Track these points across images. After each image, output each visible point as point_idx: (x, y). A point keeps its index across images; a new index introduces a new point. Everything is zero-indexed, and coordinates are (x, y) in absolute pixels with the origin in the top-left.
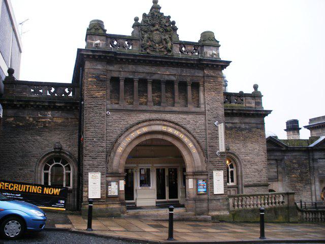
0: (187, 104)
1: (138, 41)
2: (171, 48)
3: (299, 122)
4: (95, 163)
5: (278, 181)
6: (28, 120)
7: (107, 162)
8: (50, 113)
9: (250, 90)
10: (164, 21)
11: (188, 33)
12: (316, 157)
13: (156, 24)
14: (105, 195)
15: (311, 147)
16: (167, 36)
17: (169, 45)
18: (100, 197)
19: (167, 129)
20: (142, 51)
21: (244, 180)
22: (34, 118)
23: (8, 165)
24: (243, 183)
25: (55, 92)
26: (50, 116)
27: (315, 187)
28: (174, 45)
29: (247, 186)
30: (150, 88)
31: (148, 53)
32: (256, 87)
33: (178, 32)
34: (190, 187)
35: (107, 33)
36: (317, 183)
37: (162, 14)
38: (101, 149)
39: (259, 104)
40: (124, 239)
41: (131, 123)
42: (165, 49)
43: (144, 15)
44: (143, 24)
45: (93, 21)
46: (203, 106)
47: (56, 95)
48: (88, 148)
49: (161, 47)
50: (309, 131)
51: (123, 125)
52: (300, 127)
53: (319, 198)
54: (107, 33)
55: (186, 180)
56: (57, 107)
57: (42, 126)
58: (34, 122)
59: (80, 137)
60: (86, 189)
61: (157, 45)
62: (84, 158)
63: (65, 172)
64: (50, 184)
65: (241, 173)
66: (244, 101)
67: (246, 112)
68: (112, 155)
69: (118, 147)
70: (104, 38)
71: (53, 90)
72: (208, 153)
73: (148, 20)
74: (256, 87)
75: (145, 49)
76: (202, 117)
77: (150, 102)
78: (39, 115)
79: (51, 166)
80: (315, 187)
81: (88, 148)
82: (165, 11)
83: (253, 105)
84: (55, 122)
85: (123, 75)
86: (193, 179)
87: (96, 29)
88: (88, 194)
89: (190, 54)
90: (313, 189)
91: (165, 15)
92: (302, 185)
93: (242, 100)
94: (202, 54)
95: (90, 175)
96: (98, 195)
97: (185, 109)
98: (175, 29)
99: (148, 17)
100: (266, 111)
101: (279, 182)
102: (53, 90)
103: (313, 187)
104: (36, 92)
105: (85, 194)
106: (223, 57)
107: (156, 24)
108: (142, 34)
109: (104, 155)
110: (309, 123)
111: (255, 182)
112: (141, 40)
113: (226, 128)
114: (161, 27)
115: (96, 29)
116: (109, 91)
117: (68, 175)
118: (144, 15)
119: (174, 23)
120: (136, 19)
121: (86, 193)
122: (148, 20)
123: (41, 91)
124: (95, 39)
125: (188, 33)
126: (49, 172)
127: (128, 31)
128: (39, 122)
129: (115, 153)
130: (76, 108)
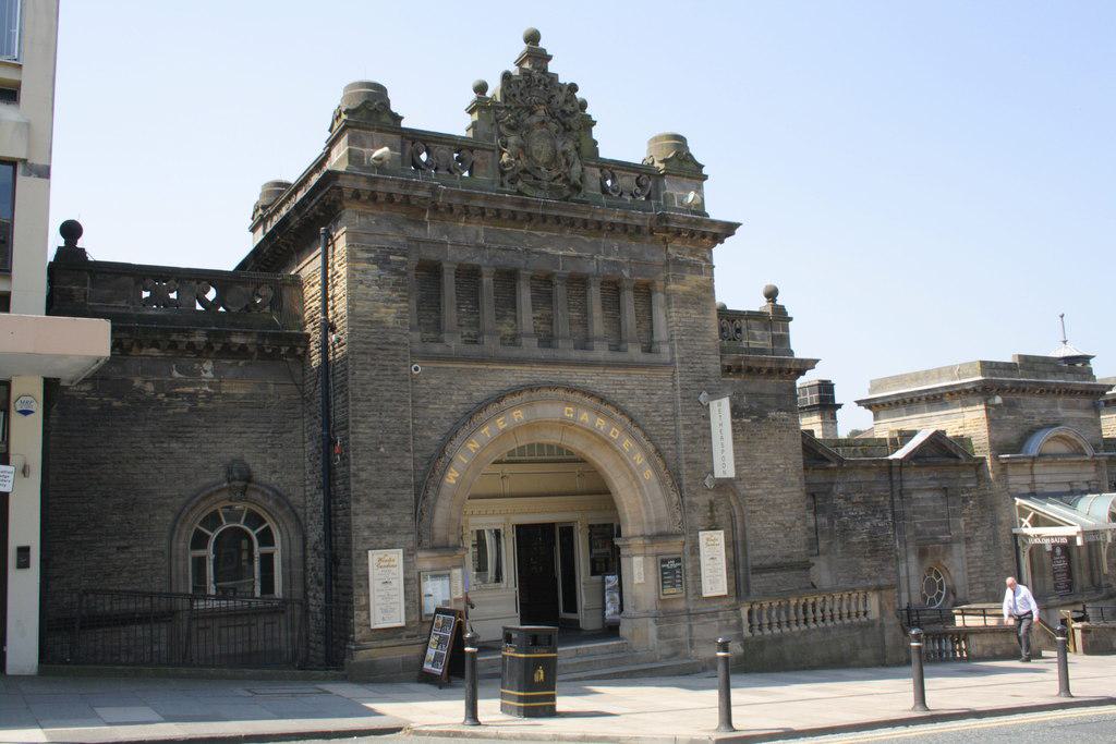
0: (621, 341)
1: (490, 154)
2: (580, 179)
3: (836, 389)
4: (387, 520)
5: (818, 554)
6: (141, 391)
7: (418, 516)
8: (208, 366)
9: (758, 304)
10: (561, 98)
11: (622, 137)
12: (908, 485)
13: (535, 102)
14: (415, 617)
15: (901, 461)
16: (570, 146)
17: (577, 168)
18: (403, 624)
19: (576, 415)
20: (502, 185)
21: (749, 553)
22: (159, 387)
23: (79, 538)
24: (749, 564)
25: (219, 301)
26: (210, 375)
27: (907, 568)
28: (587, 168)
29: (760, 570)
30: (525, 295)
31: (519, 192)
32: (772, 294)
33: (596, 133)
34: (637, 580)
35: (404, 124)
36: (913, 558)
37: (554, 77)
38: (401, 479)
39: (783, 340)
40: (523, 737)
41: (479, 396)
42: (564, 181)
43: (507, 76)
44: (503, 105)
45: (353, 86)
46: (665, 349)
47: (221, 309)
48: (363, 475)
49: (554, 174)
50: (870, 414)
51: (457, 401)
52: (837, 402)
53: (916, 599)
54: (404, 124)
55: (623, 561)
56: (235, 349)
57: (185, 410)
58: (161, 396)
59: (329, 443)
60: (363, 601)
61: (543, 169)
62: (354, 506)
63: (258, 550)
64: (212, 591)
65: (744, 535)
66: (744, 332)
67: (757, 357)
68: (431, 494)
69: (446, 469)
70: (396, 139)
71: (211, 295)
72: (684, 482)
73: (517, 92)
74: (772, 294)
75: (513, 181)
76: (665, 374)
77: (528, 335)
78: (176, 374)
79: (213, 536)
80: (907, 568)
81: (363, 475)
82: (563, 69)
83: (768, 344)
84: (227, 395)
85: (452, 257)
86: (645, 555)
87: (368, 112)
88: (369, 617)
89: (629, 198)
90: (903, 573)
91: (561, 81)
92: (876, 563)
93: (738, 331)
94: (658, 198)
95: (374, 557)
96: (397, 619)
97: (619, 356)
98: (589, 123)
99: (517, 82)
100: (802, 361)
101: (822, 557)
102: (211, 295)
103: (903, 566)
104: (159, 298)
105: (359, 617)
106: (716, 211)
107: (535, 102)
108: (501, 135)
109: (409, 493)
110: (871, 391)
111: (778, 559)
112: (497, 152)
113: (736, 412)
114: (553, 116)
115: (368, 112)
116: (413, 302)
117: (267, 560)
118: (507, 76)
119: (583, 105)
120: (481, 88)
121: (364, 614)
122: (517, 92)
123: (173, 296)
124: (368, 142)
125: (622, 137)
126: (209, 553)
127: (456, 122)
128: (177, 395)
129: (439, 487)
130: (292, 351)
